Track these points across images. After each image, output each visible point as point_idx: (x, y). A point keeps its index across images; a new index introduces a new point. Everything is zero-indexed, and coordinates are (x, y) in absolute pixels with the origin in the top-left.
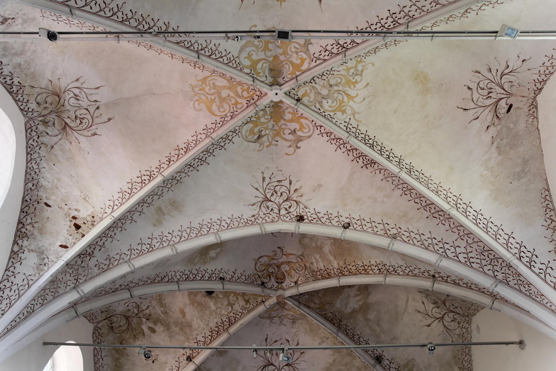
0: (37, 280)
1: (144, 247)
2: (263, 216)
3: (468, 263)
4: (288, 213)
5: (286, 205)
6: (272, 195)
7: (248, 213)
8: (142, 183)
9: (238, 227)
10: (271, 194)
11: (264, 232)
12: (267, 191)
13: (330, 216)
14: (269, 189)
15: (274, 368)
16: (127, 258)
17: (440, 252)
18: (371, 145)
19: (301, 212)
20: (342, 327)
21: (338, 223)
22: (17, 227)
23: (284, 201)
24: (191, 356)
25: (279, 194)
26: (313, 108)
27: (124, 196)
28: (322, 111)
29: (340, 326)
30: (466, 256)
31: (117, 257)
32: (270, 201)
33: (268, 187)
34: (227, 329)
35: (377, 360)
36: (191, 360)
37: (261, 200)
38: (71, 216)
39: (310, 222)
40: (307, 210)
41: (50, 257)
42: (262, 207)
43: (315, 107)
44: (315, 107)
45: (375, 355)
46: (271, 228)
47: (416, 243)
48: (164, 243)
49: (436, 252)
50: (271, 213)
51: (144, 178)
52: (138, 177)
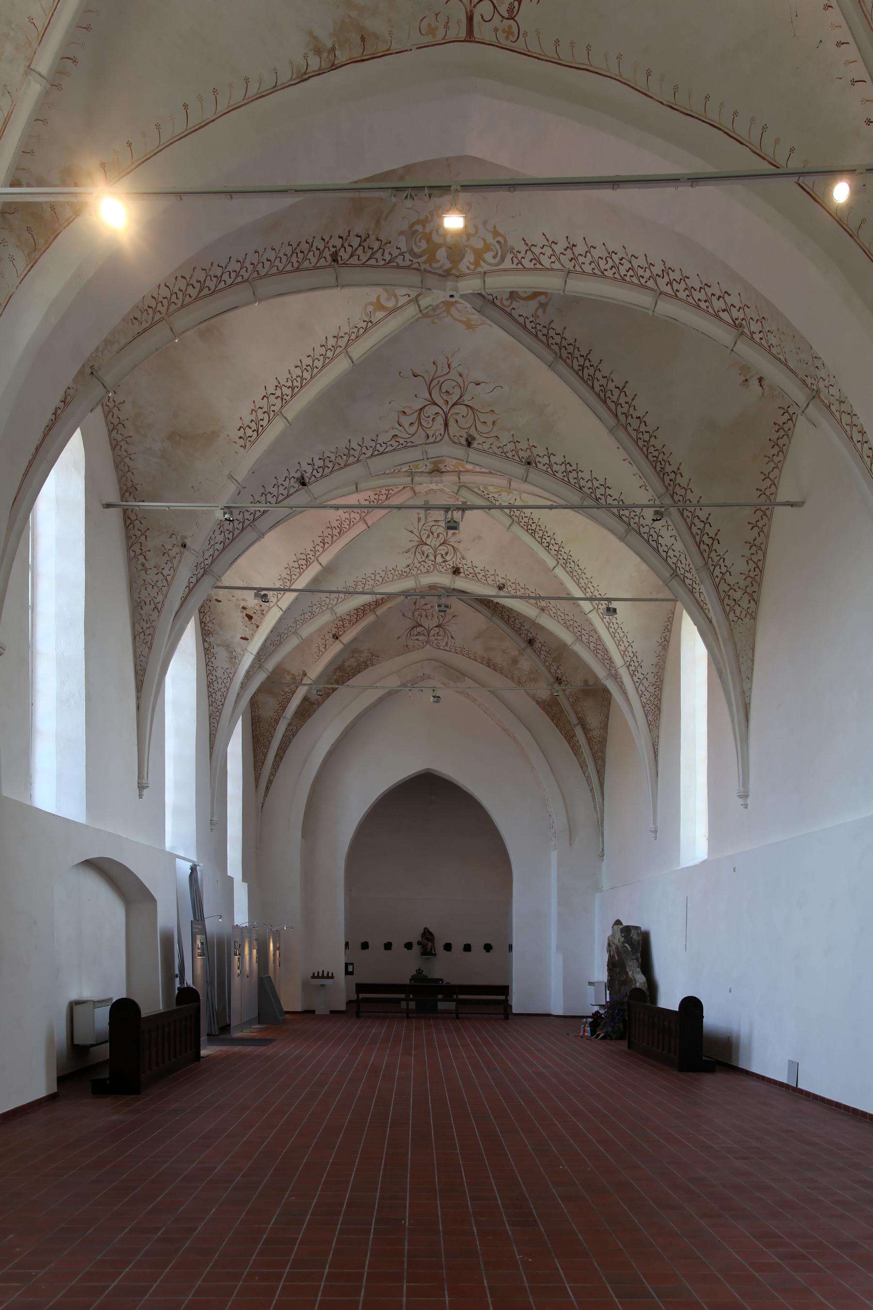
0: (235, 673)
1: (306, 616)
2: (418, 565)
3: (595, 652)
4: (444, 562)
5: (443, 550)
6: (428, 536)
7: (402, 562)
8: (299, 568)
9: (392, 580)
10: (426, 535)
11: (418, 586)
12: (423, 532)
13: (487, 572)
14: (425, 530)
15: (423, 629)
16: (293, 630)
17: (577, 635)
18: (533, 531)
19: (457, 562)
20: (498, 610)
21: (494, 582)
22: (201, 626)
23: (440, 545)
24: (337, 634)
25: (436, 535)
26: (476, 490)
27: (285, 584)
28: (486, 493)
29: (496, 609)
30: (595, 646)
31: (286, 631)
32: (426, 544)
33: (424, 528)
34: (374, 609)
35: (529, 643)
36: (337, 638)
37: (416, 543)
38: (241, 607)
39: (466, 576)
40: (464, 562)
41: (236, 650)
42: (417, 553)
43: (479, 489)
44: (479, 489)
45: (528, 638)
46: (427, 580)
47: (560, 620)
48: (323, 607)
49: (574, 633)
50: (427, 560)
51: (301, 562)
52: (294, 562)
